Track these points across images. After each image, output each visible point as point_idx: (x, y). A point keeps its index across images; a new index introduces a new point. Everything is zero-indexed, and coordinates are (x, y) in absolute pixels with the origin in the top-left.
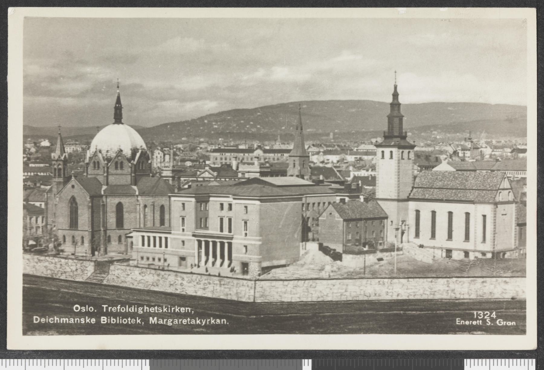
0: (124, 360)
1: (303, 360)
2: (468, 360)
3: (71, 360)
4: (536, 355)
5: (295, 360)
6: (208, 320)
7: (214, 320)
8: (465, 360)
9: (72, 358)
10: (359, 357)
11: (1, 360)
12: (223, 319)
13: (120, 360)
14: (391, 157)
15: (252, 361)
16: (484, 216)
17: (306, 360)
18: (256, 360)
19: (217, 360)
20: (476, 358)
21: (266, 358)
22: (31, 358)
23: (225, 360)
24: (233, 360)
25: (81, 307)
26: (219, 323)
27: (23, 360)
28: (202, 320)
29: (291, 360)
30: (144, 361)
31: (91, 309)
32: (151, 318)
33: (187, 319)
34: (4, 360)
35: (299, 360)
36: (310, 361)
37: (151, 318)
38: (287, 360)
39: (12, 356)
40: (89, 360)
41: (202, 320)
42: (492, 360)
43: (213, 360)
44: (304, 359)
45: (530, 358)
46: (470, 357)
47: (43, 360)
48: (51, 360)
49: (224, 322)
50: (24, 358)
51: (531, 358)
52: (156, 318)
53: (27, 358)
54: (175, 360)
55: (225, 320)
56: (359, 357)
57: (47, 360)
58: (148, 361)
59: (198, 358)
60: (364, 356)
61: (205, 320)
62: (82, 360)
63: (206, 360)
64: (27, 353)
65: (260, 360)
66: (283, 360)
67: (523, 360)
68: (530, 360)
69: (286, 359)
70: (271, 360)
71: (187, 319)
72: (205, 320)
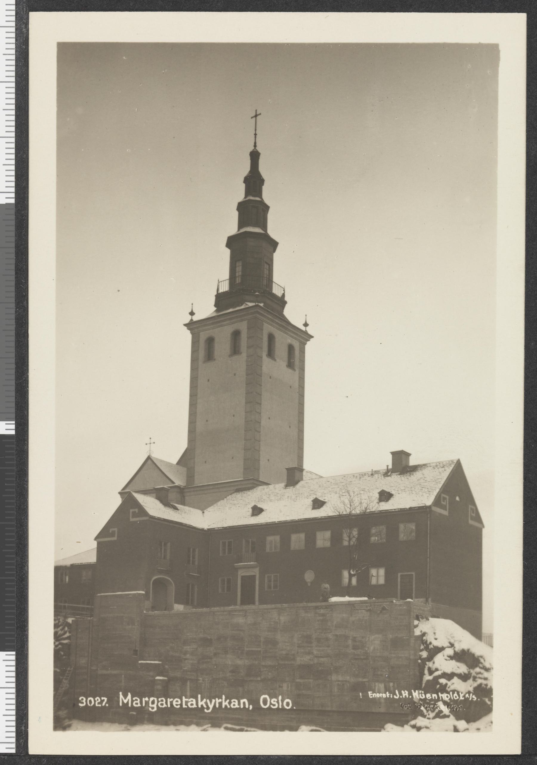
14: (235, 350)
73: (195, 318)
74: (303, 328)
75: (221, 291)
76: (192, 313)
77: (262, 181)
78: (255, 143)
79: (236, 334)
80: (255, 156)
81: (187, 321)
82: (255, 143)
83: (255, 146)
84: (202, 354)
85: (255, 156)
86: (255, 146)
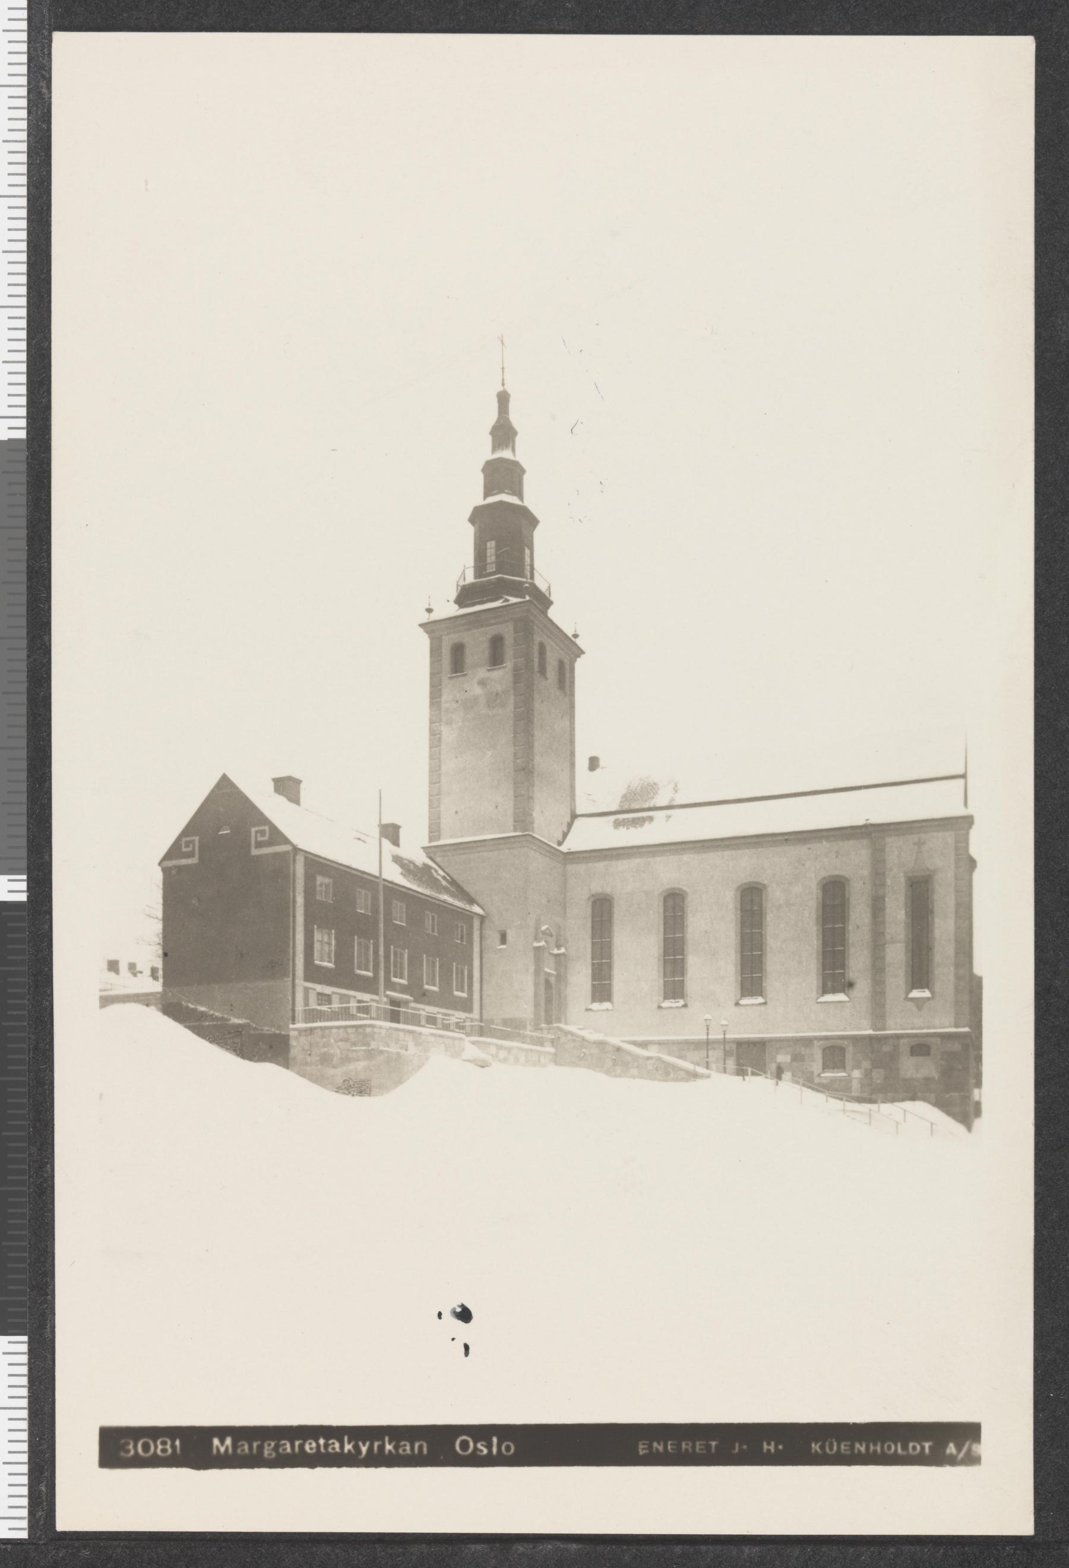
0: (23, 368)
1: (25, 877)
2: (24, 1348)
3: (25, 216)
4: (40, 1539)
5: (24, 853)
6: (376, 1444)
7: (394, 1443)
8: (25, 1338)
9: (29, 274)
10: (33, 1037)
11: (25, 4)
12: (913, 1441)
13: (24, 357)
15: (23, 732)
17: (24, 886)
18: (24, 743)
19: (24, 632)
20: (30, 1370)
21: (29, 771)
22: (29, 101)
23: (24, 654)
24: (23, 677)
25: (475, 1443)
26: (338, 1450)
27: (24, 80)
28: (361, 1444)
29: (24, 842)
30: (23, 423)
31: (508, 1448)
32: (216, 1442)
33: (317, 1441)
34: (24, 14)
35: (24, 864)
36: (23, 897)
37: (216, 1442)
38: (24, 831)
39: (35, 49)
40: (24, 1381)
41: (361, 1444)
42: (25, 1414)
43: (25, 631)
44: (29, 881)
45: (29, 1522)
46: (31, 1353)
47: (24, 136)
48: (24, 158)
49: (421, 1447)
50: (29, 83)
51: (32, 1527)
52: (228, 1441)
53: (29, 92)
54: (23, 511)
55: (425, 1445)
56: (33, 1037)
57: (24, 147)
58: (22, 435)
59: (29, 579)
60: (36, 1049)
61: (368, 1444)
62: (25, 249)
63: (24, 599)
64: (44, 90)
65: (24, 754)
66: (24, 820)
67: (25, 1502)
68: (25, 1524)
69: (28, 829)
70: (24, 787)
71: (317, 1441)
72: (368, 1444)
78: (503, 380)
80: (503, 399)
82: (503, 380)
83: (503, 385)
85: (503, 399)
86: (503, 385)
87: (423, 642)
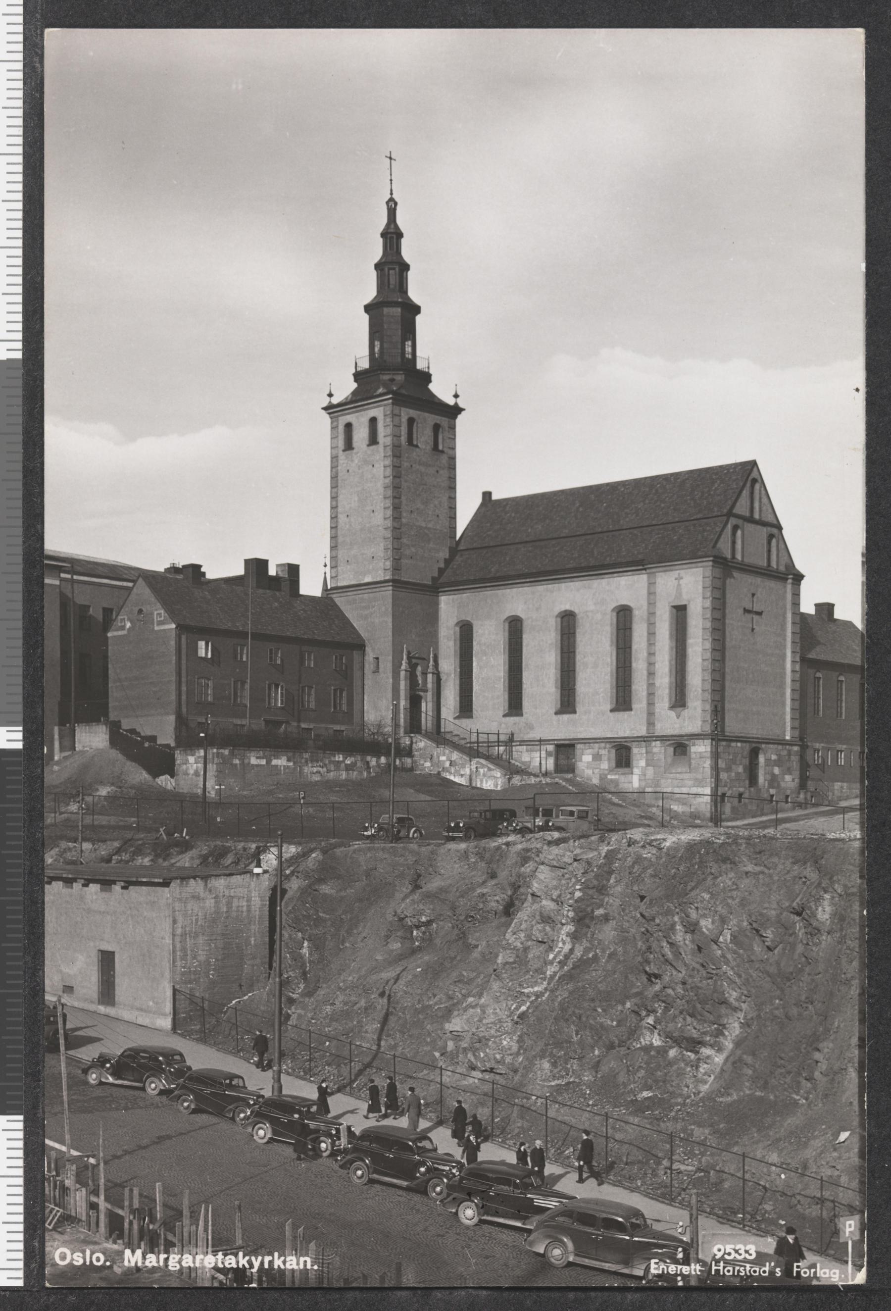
14: (373, 440)
16: (680, 612)
73: (335, 400)
74: (451, 401)
75: (359, 369)
76: (330, 395)
77: (400, 235)
78: (391, 190)
79: (373, 421)
81: (325, 404)
82: (391, 190)
83: (391, 194)
84: (341, 443)
86: (391, 194)
87: (325, 419)
